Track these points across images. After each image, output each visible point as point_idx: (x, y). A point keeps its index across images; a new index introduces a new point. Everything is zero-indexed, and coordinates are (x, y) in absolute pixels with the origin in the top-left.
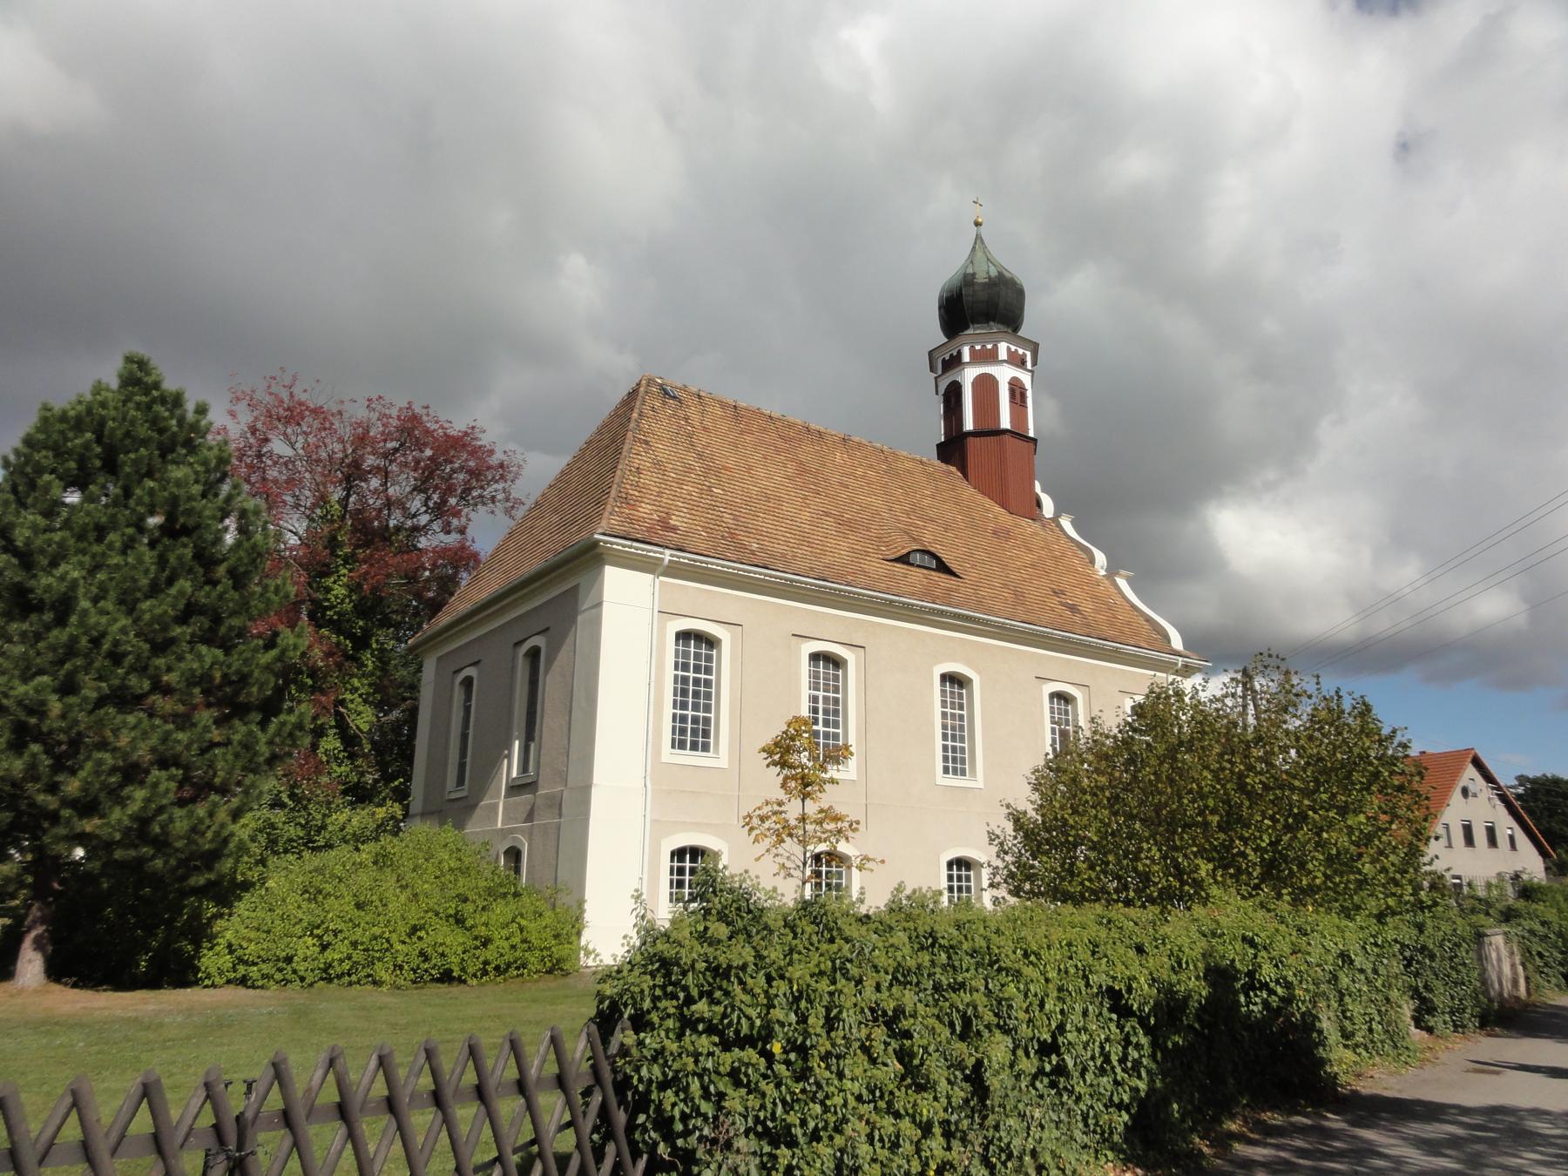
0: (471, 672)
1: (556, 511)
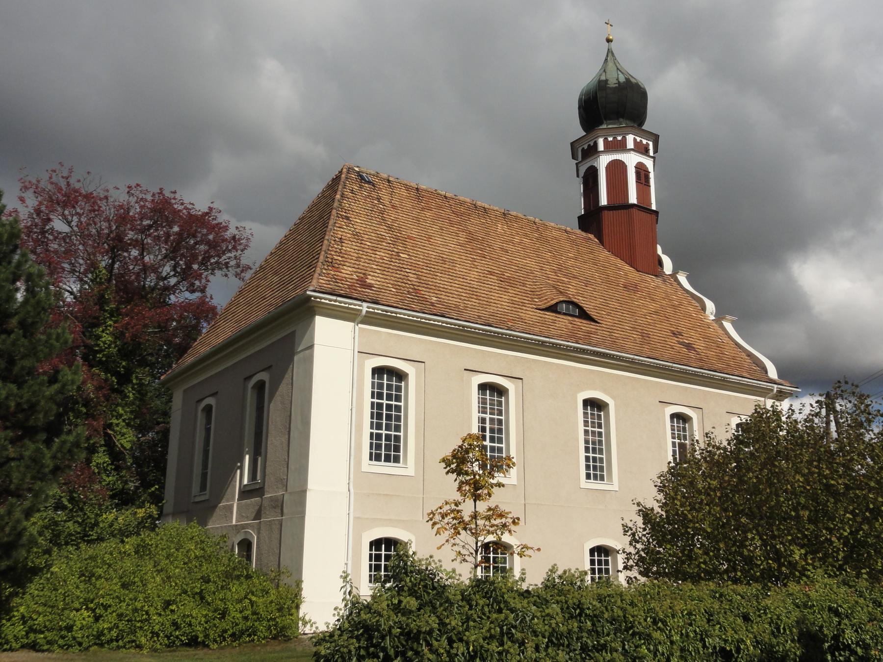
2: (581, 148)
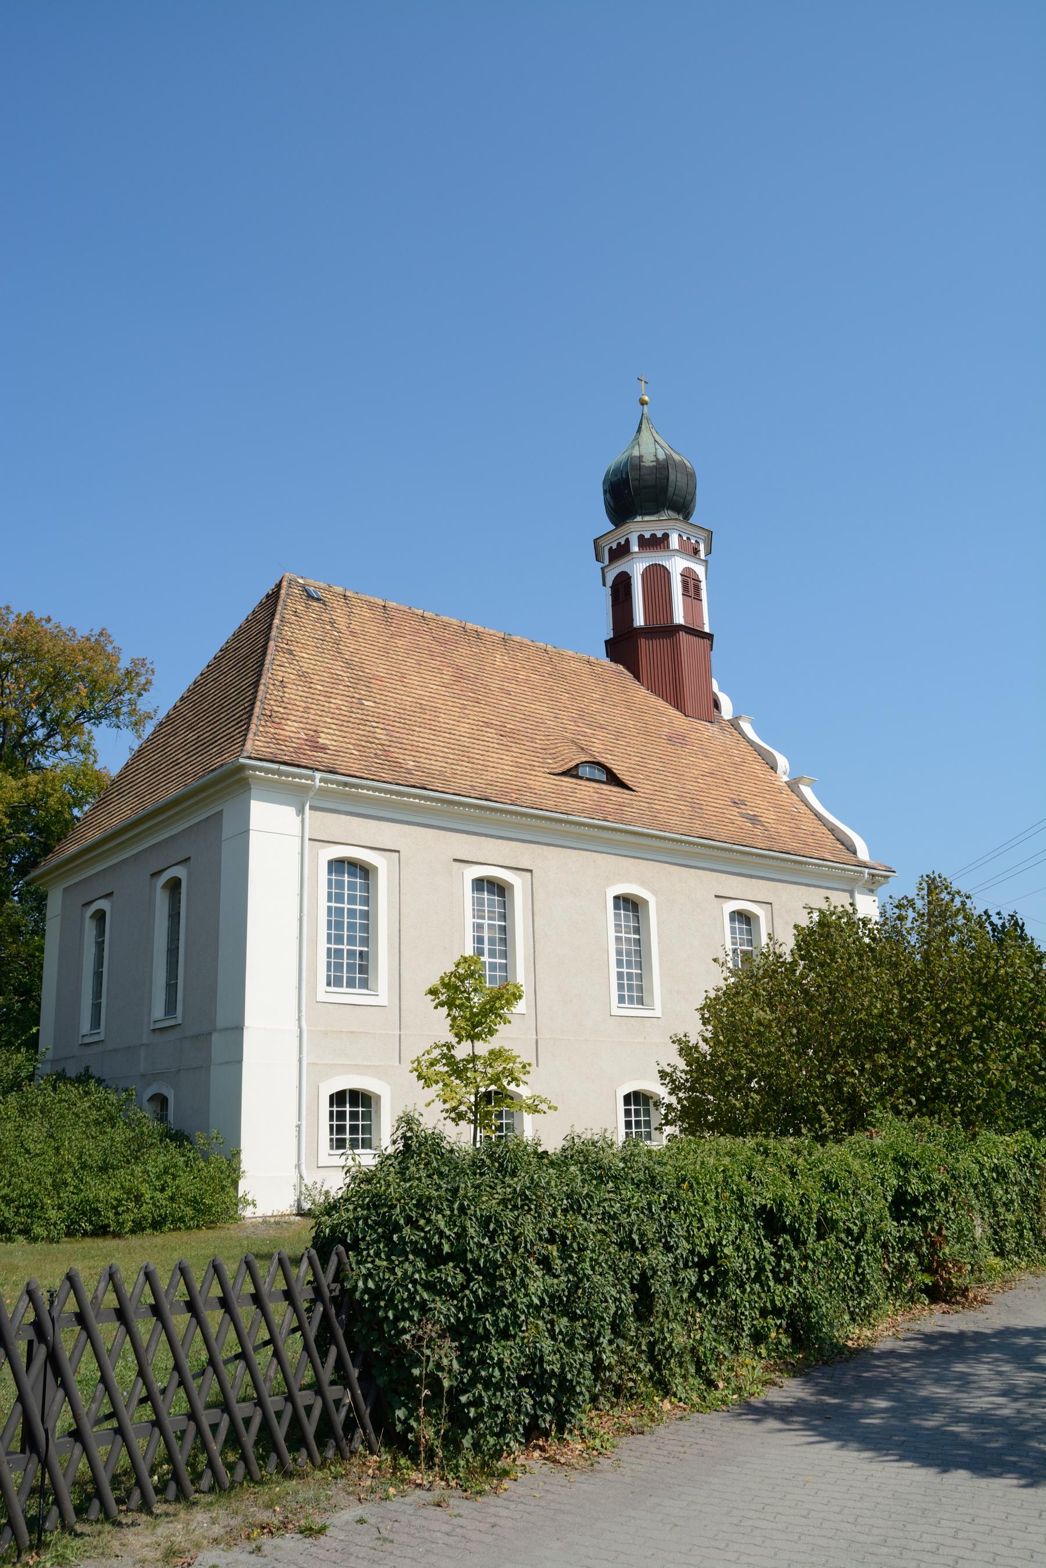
0: (103, 904)
1: (191, 728)
2: (608, 547)
